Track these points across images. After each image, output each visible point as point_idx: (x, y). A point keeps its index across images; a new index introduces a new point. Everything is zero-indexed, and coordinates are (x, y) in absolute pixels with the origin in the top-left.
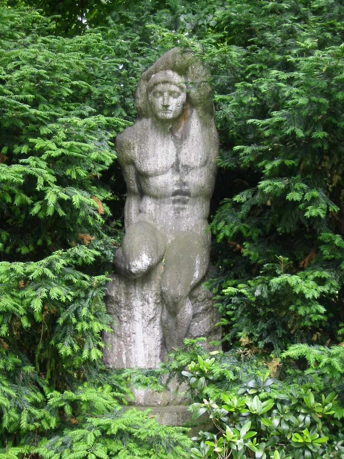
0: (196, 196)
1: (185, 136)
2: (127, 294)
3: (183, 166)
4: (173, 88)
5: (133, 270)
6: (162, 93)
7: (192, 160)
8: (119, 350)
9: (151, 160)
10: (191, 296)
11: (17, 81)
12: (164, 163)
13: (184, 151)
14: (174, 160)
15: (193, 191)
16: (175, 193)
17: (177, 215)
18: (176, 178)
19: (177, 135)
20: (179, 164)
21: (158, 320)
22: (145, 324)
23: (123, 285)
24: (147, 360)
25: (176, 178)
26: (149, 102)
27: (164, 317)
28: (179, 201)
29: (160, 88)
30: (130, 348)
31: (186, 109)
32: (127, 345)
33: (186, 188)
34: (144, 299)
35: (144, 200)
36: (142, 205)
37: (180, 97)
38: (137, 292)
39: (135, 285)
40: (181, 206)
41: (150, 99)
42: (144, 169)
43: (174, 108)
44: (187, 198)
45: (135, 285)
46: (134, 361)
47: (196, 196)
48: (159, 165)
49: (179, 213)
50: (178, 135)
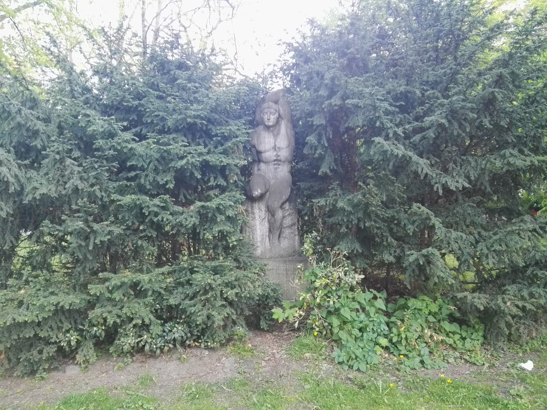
1: (278, 134)
2: (252, 207)
4: (272, 110)
10: (281, 207)
11: (420, 141)
13: (278, 140)
15: (283, 159)
16: (275, 160)
18: (275, 153)
23: (250, 203)
34: (260, 209)
47: (284, 162)
50: (275, 133)
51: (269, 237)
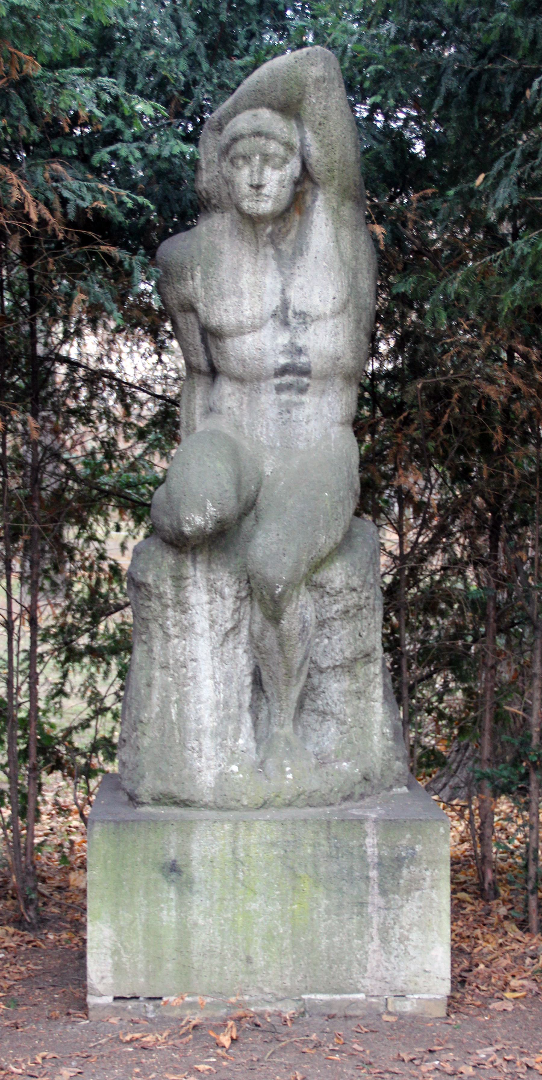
0: (325, 377)
1: (299, 250)
2: (179, 580)
3: (295, 313)
4: (273, 147)
5: (187, 529)
6: (247, 158)
7: (316, 300)
8: (164, 694)
9: (230, 302)
12: (257, 310)
13: (298, 281)
14: (276, 301)
16: (283, 371)
17: (286, 416)
18: (284, 339)
19: (283, 247)
20: (287, 309)
21: (244, 633)
22: (218, 640)
24: (222, 714)
25: (284, 339)
26: (223, 177)
27: (256, 628)
28: (289, 387)
29: (241, 147)
30: (185, 689)
31: (304, 193)
32: (181, 684)
33: (303, 359)
34: (212, 589)
35: (217, 386)
36: (215, 397)
37: (287, 166)
38: (199, 574)
39: (194, 561)
40: (295, 398)
41: (224, 171)
42: (214, 322)
43: (274, 190)
44: (305, 380)
45: (194, 561)
46: (193, 717)
47: (325, 377)
48: (247, 313)
49: (289, 412)
51: (254, 710)
